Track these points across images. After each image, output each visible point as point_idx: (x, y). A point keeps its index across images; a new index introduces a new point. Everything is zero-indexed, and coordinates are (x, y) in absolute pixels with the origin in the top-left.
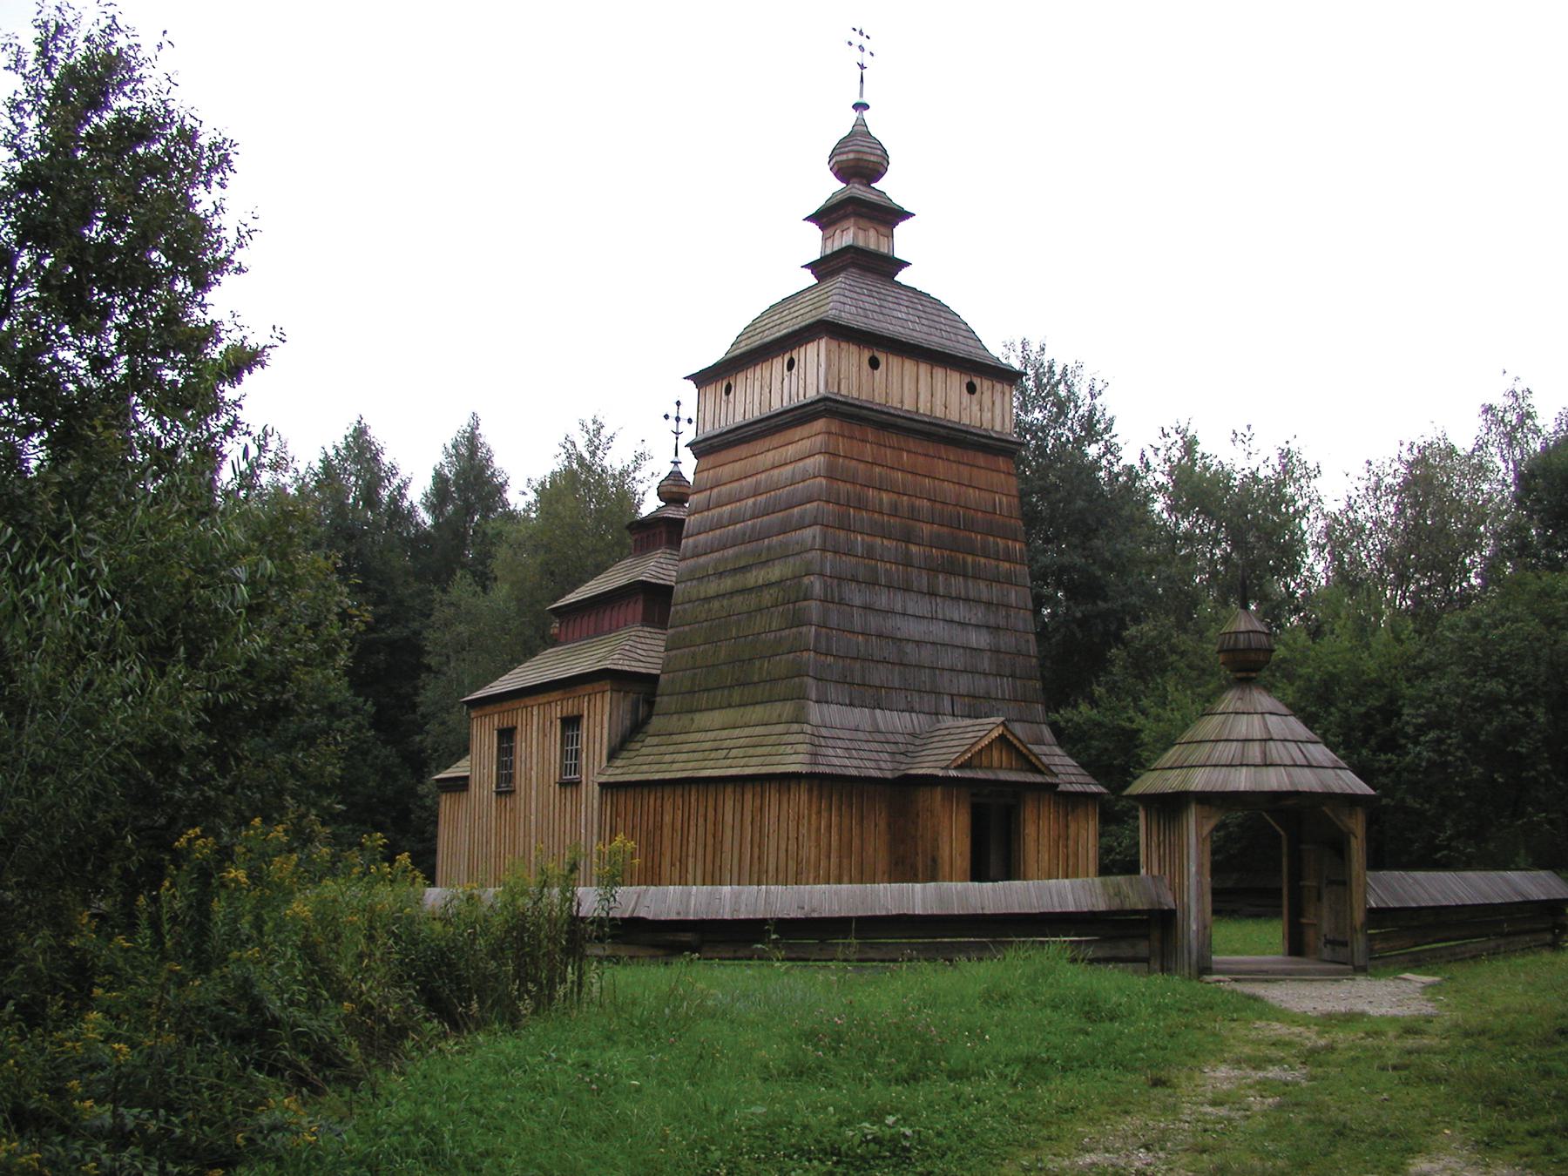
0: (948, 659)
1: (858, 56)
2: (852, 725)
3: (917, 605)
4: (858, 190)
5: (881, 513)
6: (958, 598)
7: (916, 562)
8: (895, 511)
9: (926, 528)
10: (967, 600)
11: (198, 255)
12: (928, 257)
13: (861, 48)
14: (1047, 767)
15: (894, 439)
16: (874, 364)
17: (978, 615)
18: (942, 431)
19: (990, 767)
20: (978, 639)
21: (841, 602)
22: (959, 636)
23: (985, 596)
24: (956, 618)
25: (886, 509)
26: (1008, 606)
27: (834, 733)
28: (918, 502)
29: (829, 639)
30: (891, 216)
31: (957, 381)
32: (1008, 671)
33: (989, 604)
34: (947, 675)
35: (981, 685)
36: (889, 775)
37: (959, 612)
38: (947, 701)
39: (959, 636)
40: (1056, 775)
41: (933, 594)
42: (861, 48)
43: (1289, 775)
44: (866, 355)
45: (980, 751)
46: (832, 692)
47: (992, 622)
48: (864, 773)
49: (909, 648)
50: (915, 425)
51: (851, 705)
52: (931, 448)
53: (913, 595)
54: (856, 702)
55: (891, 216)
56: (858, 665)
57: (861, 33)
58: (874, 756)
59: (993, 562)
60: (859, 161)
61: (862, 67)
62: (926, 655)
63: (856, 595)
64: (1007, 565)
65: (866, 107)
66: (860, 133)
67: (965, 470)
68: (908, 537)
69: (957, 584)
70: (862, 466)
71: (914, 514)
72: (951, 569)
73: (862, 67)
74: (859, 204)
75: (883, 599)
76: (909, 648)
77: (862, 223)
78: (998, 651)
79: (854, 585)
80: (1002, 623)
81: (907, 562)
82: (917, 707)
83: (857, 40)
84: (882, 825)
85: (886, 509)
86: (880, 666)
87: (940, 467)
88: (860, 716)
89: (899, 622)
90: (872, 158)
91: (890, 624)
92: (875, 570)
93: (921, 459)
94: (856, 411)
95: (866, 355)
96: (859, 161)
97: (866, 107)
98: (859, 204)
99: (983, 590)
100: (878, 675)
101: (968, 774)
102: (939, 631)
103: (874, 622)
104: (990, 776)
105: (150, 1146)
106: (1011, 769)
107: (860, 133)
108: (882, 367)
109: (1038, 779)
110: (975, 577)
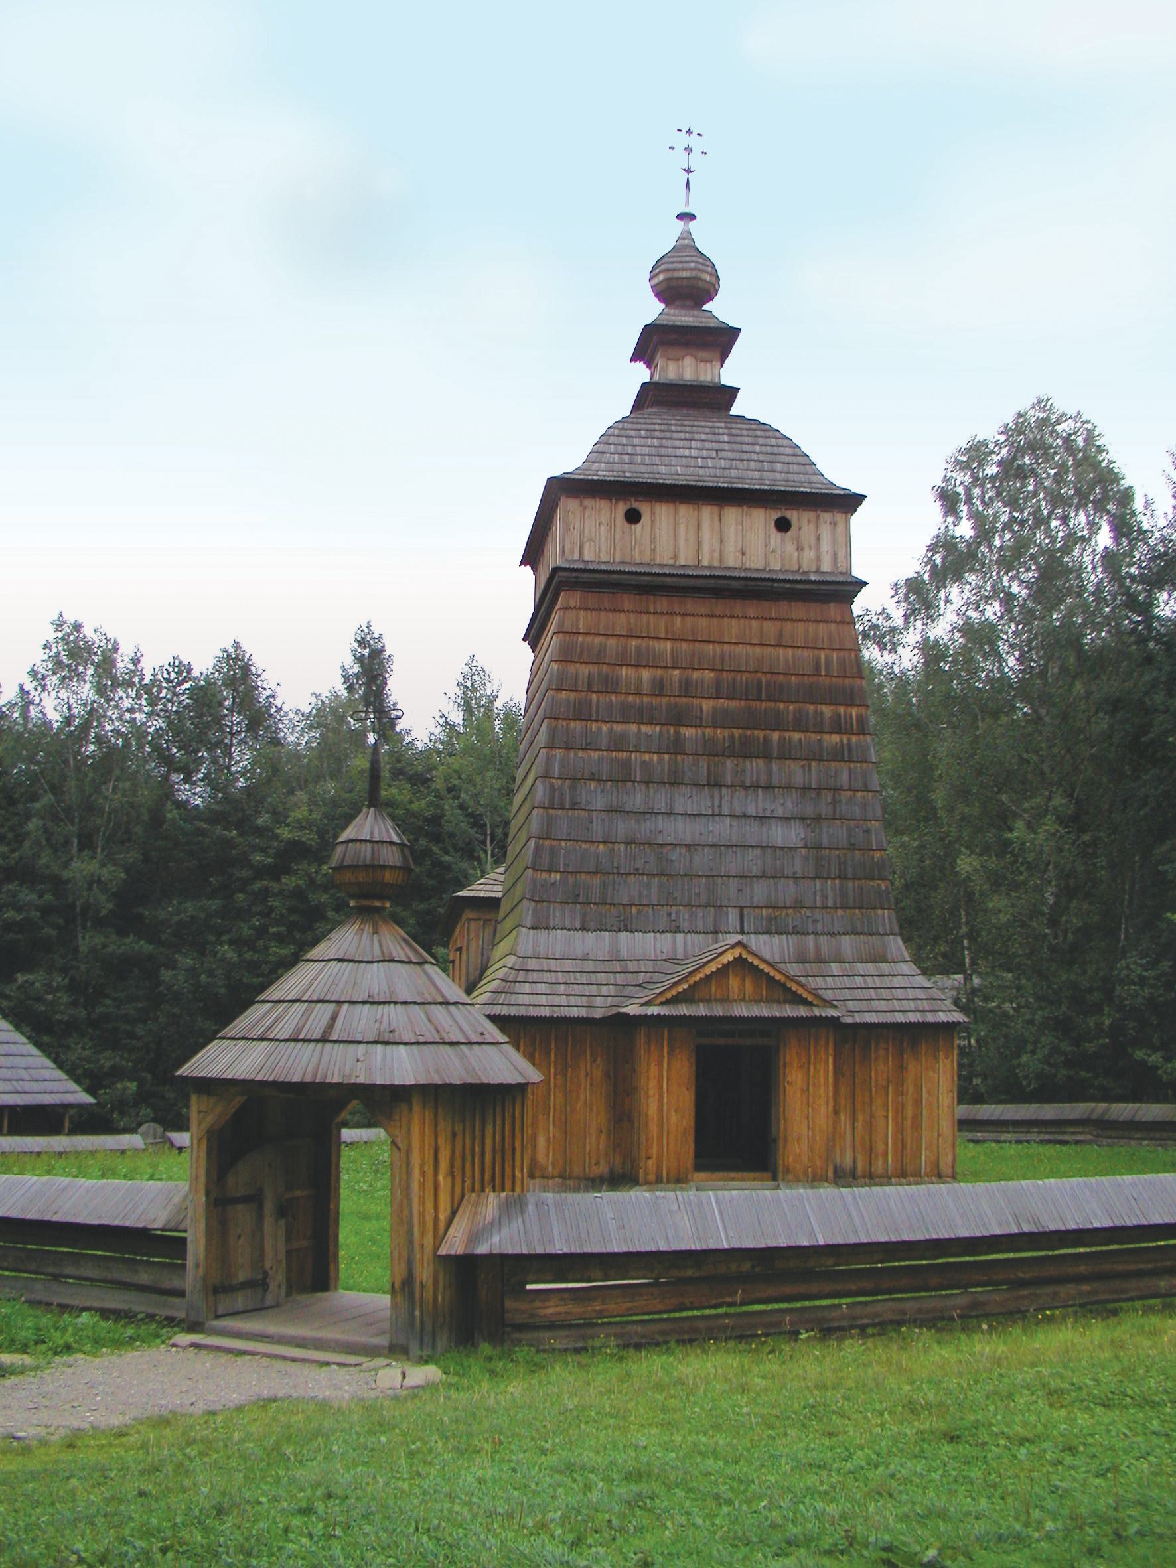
0: (733, 863)
1: (682, 160)
2: (579, 953)
3: (685, 800)
4: (685, 318)
5: (638, 694)
6: (756, 786)
7: (688, 748)
8: (659, 688)
9: (707, 705)
10: (768, 787)
11: (1114, 478)
12: (757, 382)
13: (688, 150)
14: (814, 992)
15: (662, 604)
16: (633, 517)
17: (785, 805)
18: (734, 583)
19: (725, 1000)
20: (793, 835)
21: (574, 806)
22: (753, 833)
23: (799, 779)
24: (751, 810)
25: (646, 688)
26: (837, 789)
27: (545, 965)
28: (696, 675)
29: (553, 852)
30: (722, 340)
31: (760, 520)
32: (834, 871)
33: (805, 789)
34: (733, 884)
35: (788, 891)
36: (598, 1013)
37: (756, 804)
38: (733, 916)
39: (753, 833)
40: (830, 1004)
41: (715, 783)
42: (688, 150)
43: (462, 1057)
44: (622, 508)
45: (708, 978)
46: (556, 914)
47: (809, 811)
48: (559, 1012)
49: (675, 855)
50: (700, 582)
51: (583, 929)
52: (720, 606)
53: (686, 790)
54: (592, 925)
55: (722, 340)
56: (597, 880)
57: (689, 132)
58: (587, 990)
59: (814, 737)
60: (685, 281)
61: (688, 171)
62: (702, 861)
63: (597, 797)
64: (835, 738)
65: (692, 217)
66: (686, 247)
67: (771, 628)
68: (679, 718)
69: (755, 768)
70: (612, 642)
71: (687, 688)
72: (744, 751)
73: (688, 171)
74: (686, 327)
75: (637, 799)
76: (675, 855)
77: (673, 352)
78: (818, 847)
79: (593, 784)
80: (825, 810)
81: (676, 747)
82: (685, 925)
83: (683, 140)
84: (598, 1073)
85: (646, 688)
86: (631, 879)
87: (733, 628)
88: (595, 943)
89: (661, 823)
90: (684, 274)
91: (646, 828)
92: (627, 764)
93: (704, 622)
94: (605, 576)
95: (622, 508)
96: (685, 281)
97: (692, 217)
98: (686, 327)
99: (796, 772)
100: (628, 890)
101: (683, 1010)
102: (724, 830)
103: (622, 827)
104: (719, 1011)
105: (339, 1364)
106: (757, 1001)
107: (686, 247)
108: (646, 519)
109: (802, 1011)
110: (782, 757)
